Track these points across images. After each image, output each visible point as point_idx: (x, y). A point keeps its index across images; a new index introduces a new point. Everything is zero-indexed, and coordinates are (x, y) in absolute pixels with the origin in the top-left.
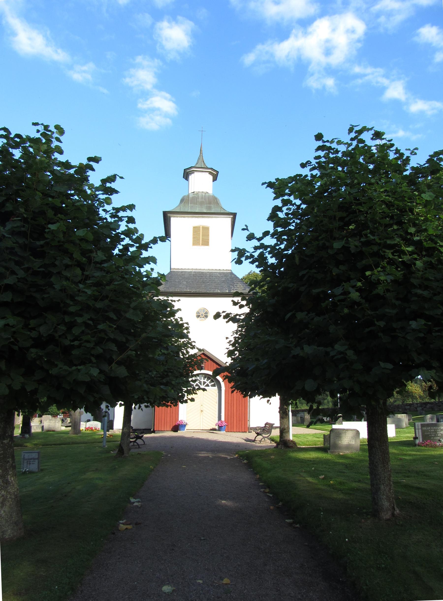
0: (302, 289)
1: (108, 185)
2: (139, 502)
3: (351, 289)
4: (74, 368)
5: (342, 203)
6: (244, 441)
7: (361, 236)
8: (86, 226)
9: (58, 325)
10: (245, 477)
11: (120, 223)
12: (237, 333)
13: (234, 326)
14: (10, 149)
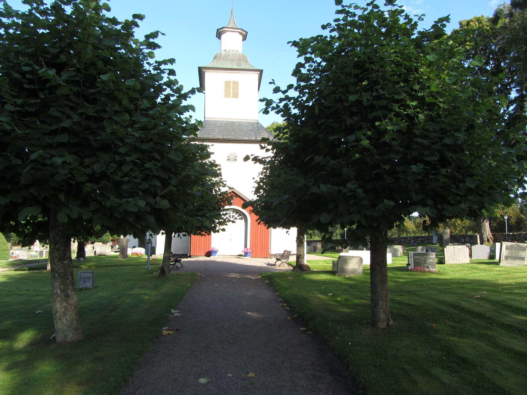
0: (320, 136)
1: (151, 40)
2: (178, 313)
3: (363, 137)
4: (124, 200)
5: (357, 62)
6: (266, 265)
7: (373, 91)
8: (132, 76)
9: (110, 163)
10: (266, 294)
11: (162, 75)
12: (262, 174)
13: (260, 167)
14: (62, 5)
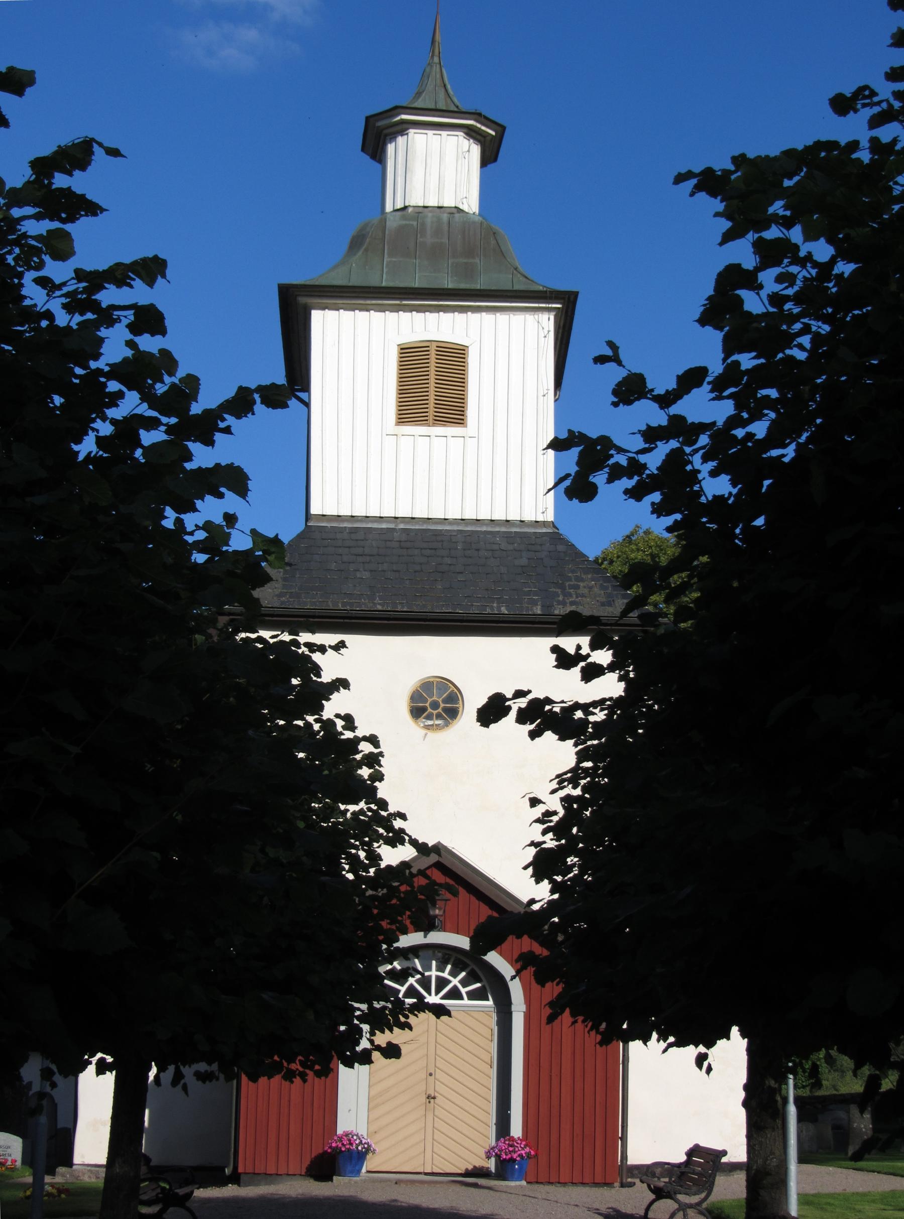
1: (60, 181)
13: (561, 754)
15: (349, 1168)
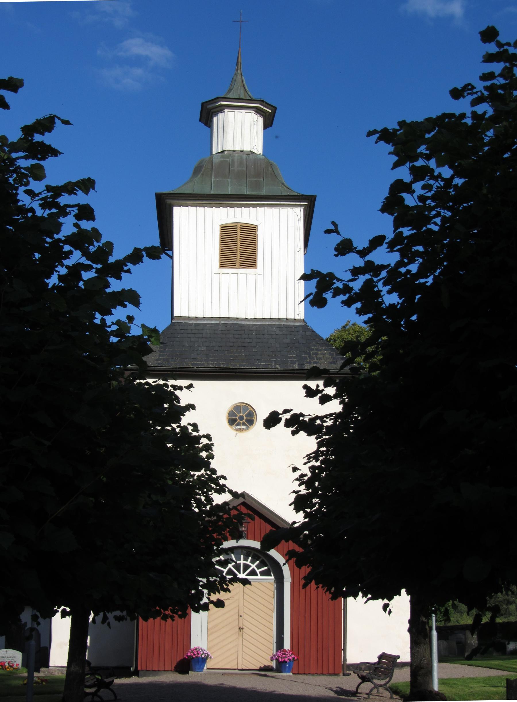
15: (197, 667)
